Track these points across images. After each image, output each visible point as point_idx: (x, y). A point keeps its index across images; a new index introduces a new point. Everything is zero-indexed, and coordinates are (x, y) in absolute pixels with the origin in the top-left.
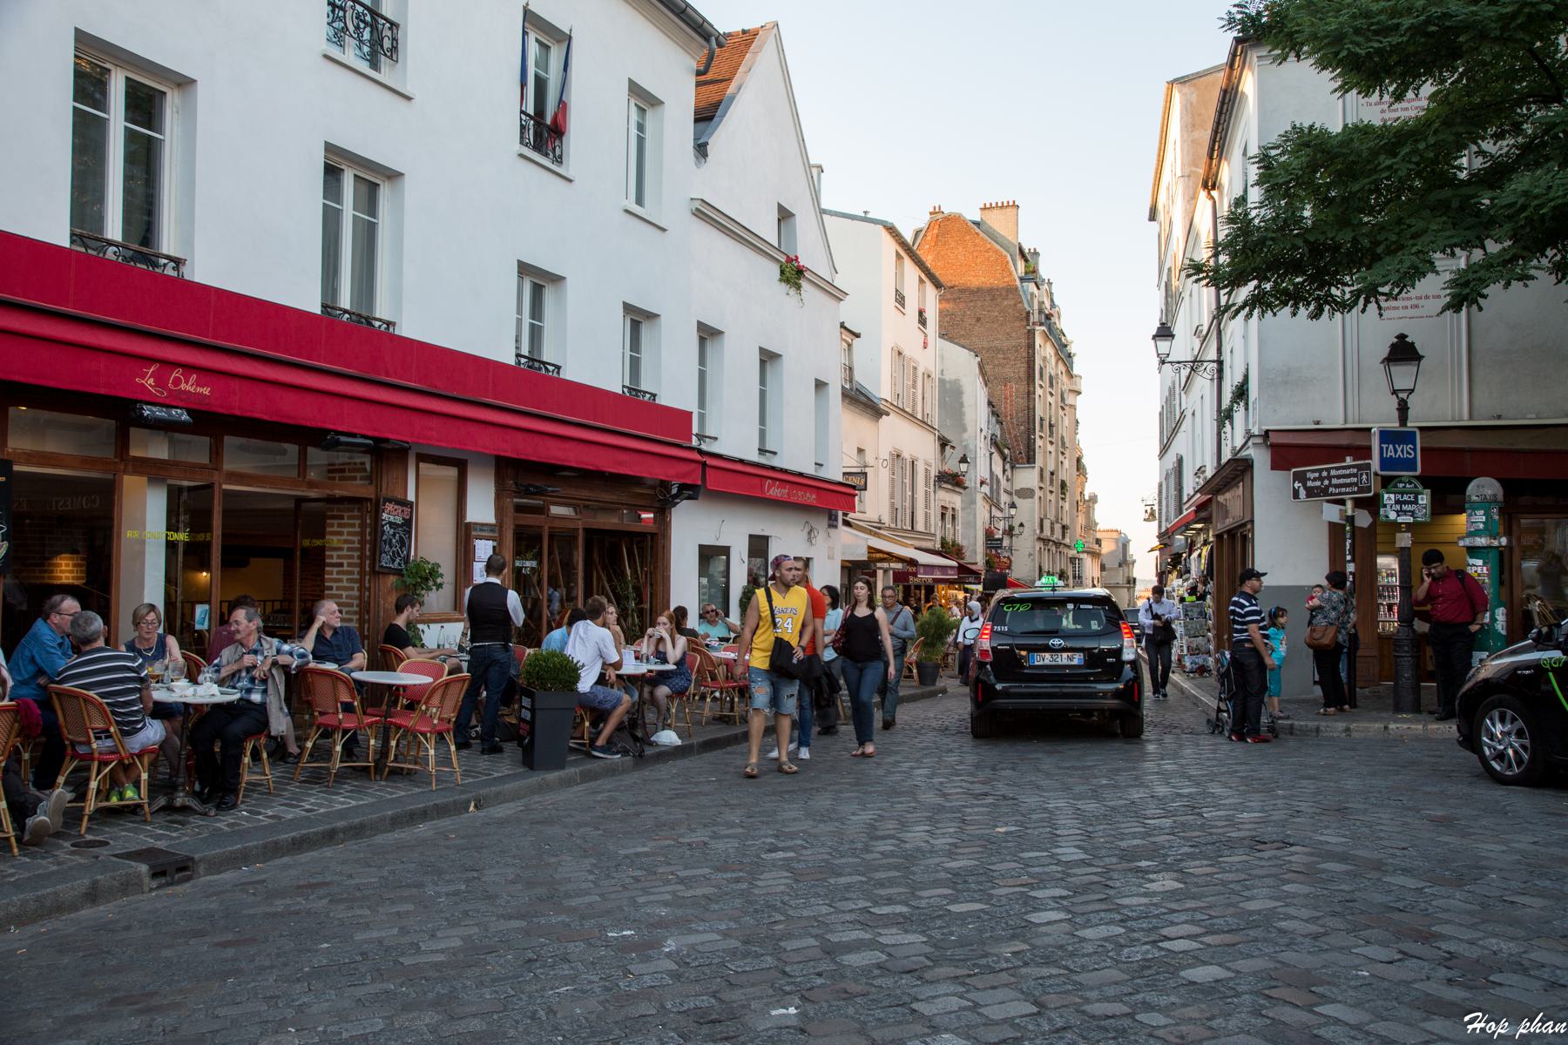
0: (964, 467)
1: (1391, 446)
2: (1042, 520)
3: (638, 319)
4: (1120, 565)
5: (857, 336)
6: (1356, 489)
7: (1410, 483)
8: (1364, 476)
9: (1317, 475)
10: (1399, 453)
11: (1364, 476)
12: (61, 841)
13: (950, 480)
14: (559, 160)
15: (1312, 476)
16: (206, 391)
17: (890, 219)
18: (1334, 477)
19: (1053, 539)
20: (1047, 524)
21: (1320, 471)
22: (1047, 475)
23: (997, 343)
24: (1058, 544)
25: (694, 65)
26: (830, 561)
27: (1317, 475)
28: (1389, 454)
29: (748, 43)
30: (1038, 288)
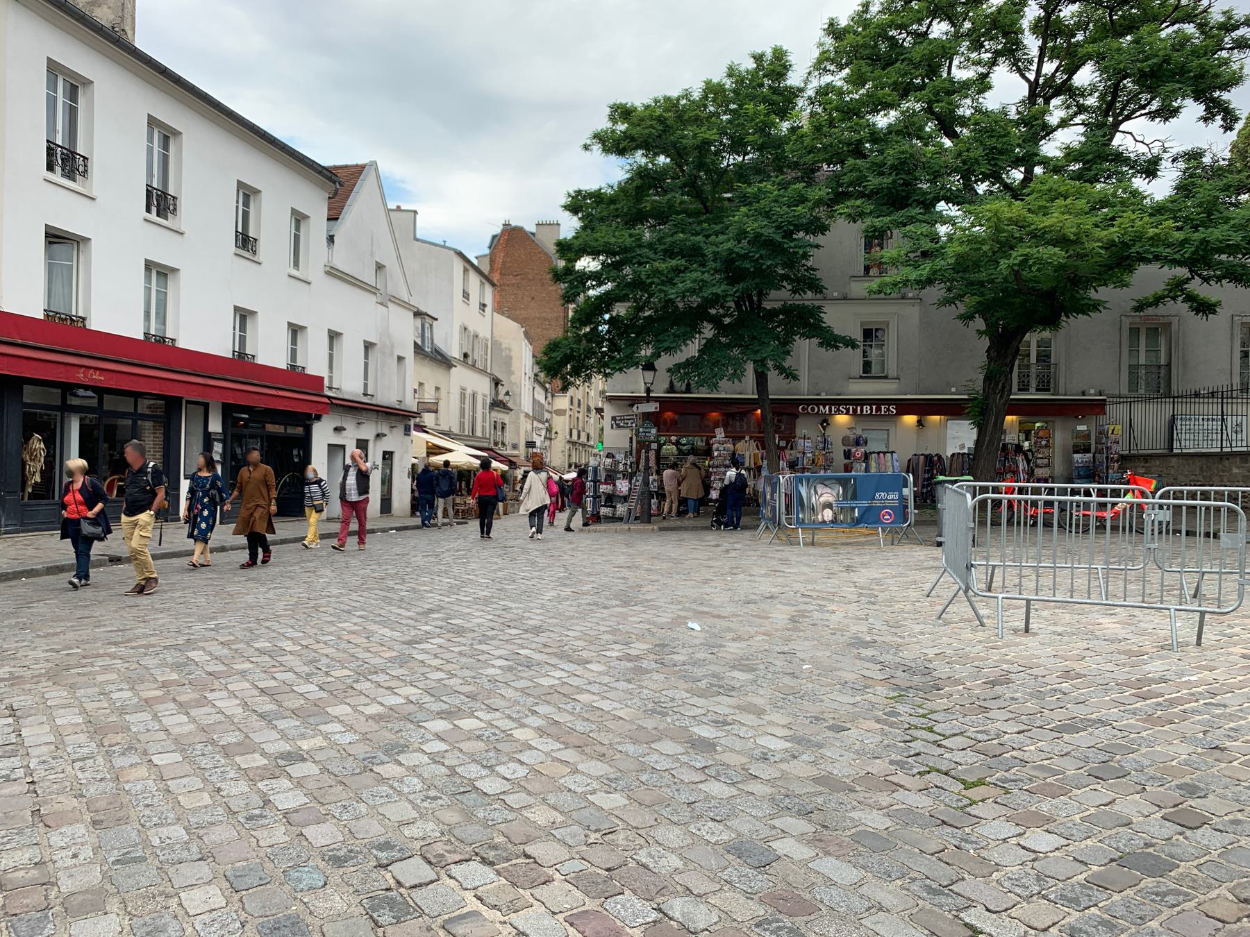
0: (507, 397)
2: (571, 430)
3: (295, 331)
5: (436, 319)
13: (497, 404)
14: (255, 253)
16: (102, 378)
17: (459, 248)
20: (575, 433)
22: (576, 402)
23: (544, 314)
24: (584, 445)
25: (327, 195)
29: (360, 173)
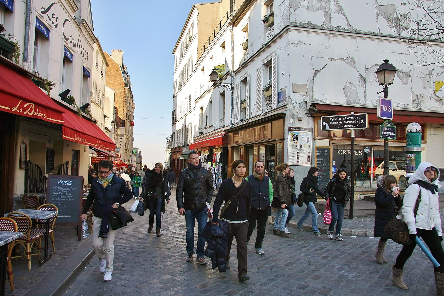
1: (384, 106)
2: (125, 144)
4: (138, 158)
6: (357, 125)
7: (390, 123)
8: (362, 120)
9: (336, 119)
10: (386, 109)
11: (362, 120)
12: (45, 112)
15: (333, 120)
18: (345, 120)
19: (128, 149)
21: (338, 117)
24: (128, 151)
26: (291, 146)
27: (336, 119)
28: (383, 109)
30: (127, 76)
